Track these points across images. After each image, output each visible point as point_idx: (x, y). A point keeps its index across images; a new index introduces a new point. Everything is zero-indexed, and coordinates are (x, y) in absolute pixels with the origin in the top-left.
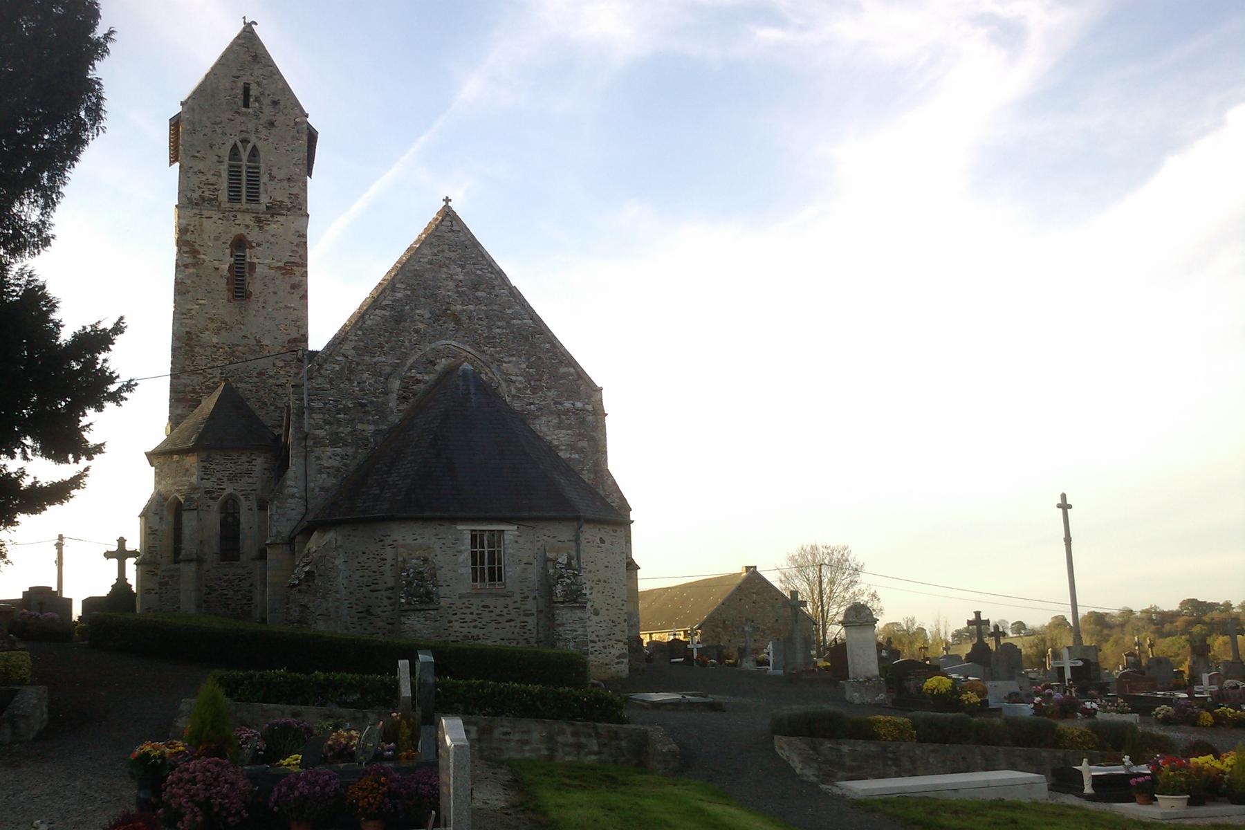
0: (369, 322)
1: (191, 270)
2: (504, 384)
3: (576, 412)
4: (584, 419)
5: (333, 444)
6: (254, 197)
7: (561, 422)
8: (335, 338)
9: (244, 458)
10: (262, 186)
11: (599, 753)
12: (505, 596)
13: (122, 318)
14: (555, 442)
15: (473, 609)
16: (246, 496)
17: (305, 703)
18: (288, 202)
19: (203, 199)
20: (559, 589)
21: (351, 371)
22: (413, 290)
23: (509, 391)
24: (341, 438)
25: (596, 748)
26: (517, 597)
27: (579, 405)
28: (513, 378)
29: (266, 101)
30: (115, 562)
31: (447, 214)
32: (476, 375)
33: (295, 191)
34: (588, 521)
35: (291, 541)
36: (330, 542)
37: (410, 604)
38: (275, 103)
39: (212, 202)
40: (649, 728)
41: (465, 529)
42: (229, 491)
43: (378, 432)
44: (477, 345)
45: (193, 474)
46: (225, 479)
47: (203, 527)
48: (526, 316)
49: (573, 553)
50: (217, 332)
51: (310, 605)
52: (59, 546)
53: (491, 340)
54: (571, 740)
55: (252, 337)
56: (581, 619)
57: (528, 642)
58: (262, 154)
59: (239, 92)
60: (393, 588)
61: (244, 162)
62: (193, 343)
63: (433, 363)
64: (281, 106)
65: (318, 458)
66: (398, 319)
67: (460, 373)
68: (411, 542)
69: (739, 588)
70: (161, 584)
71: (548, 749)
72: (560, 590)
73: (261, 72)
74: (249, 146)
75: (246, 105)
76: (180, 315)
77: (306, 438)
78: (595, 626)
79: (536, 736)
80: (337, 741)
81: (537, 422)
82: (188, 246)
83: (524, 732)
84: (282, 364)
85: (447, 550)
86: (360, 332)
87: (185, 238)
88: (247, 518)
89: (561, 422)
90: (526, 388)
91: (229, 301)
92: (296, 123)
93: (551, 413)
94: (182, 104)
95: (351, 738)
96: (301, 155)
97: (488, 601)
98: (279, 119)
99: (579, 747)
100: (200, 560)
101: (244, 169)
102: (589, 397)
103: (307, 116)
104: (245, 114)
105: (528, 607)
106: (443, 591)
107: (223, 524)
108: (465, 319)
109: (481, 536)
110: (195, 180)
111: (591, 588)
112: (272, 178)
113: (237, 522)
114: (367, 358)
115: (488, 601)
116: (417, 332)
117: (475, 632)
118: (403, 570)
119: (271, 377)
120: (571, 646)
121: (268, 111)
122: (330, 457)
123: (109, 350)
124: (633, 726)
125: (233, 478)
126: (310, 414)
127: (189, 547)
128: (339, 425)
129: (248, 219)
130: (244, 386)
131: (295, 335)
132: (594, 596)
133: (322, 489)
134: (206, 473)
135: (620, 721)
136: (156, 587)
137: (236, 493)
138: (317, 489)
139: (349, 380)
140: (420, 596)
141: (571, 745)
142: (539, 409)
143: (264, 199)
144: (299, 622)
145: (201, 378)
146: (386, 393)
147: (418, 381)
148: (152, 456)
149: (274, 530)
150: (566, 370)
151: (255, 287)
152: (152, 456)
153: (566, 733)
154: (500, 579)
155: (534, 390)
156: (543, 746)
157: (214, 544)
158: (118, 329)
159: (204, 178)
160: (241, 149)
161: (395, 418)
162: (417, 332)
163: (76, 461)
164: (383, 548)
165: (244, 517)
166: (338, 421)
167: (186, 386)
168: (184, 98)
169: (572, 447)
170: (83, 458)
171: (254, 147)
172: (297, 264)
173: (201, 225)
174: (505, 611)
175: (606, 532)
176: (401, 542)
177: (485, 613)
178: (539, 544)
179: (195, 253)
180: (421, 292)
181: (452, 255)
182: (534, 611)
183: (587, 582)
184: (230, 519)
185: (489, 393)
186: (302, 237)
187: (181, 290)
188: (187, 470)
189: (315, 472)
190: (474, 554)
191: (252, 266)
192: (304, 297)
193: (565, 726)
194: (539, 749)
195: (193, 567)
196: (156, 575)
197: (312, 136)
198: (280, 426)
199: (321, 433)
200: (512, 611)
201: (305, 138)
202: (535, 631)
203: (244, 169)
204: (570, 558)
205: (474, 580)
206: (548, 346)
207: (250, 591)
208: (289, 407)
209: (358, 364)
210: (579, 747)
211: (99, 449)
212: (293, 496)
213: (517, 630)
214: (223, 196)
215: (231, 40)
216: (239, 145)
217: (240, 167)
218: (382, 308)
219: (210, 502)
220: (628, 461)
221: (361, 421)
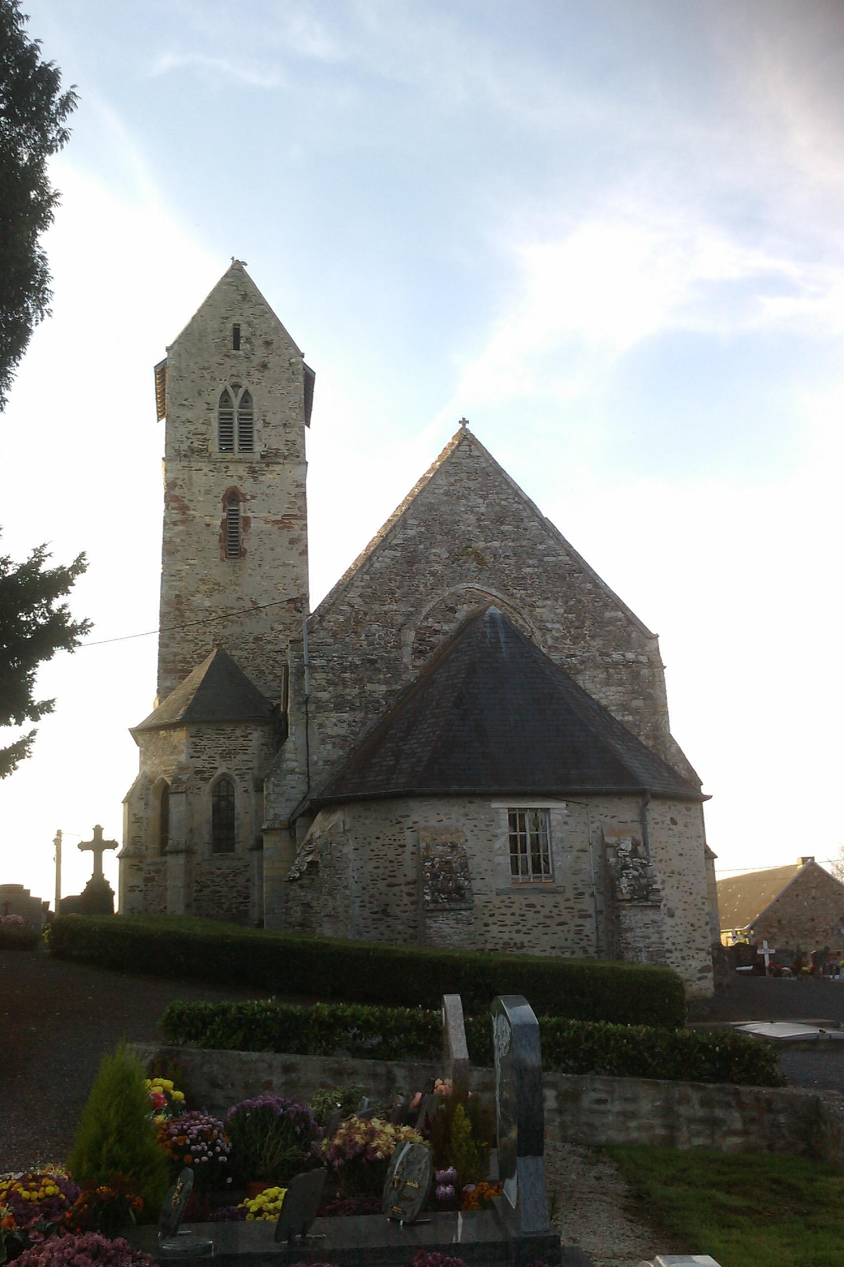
0: (377, 565)
1: (181, 528)
2: (538, 633)
3: (627, 664)
4: (638, 673)
5: (339, 708)
6: (247, 445)
7: (609, 676)
8: (339, 584)
9: (238, 733)
10: (255, 433)
11: (745, 1133)
12: (554, 892)
13: (83, 555)
14: (604, 702)
15: (515, 909)
16: (242, 776)
17: (302, 1050)
18: (284, 450)
19: (192, 450)
20: (624, 883)
21: (358, 622)
22: (428, 527)
23: (545, 642)
24: (348, 701)
25: (739, 1126)
26: (570, 894)
27: (630, 656)
28: (549, 625)
29: (257, 342)
30: (90, 854)
31: (465, 438)
32: (505, 621)
33: (291, 437)
34: (656, 796)
35: (290, 826)
36: (336, 825)
37: (435, 901)
38: (268, 343)
39: (202, 452)
40: (820, 1094)
41: (501, 807)
42: (222, 770)
43: (390, 693)
44: (504, 588)
45: (181, 752)
46: (217, 757)
47: (193, 812)
48: (561, 552)
49: (639, 837)
50: (209, 594)
51: (314, 904)
52: (58, 842)
53: (520, 581)
54: (700, 1112)
55: (247, 598)
56: (653, 922)
57: (586, 952)
58: (255, 399)
59: (229, 333)
60: (414, 882)
61: (236, 409)
62: (183, 607)
63: (453, 610)
64: (274, 346)
65: (321, 726)
66: (411, 561)
67: (486, 618)
68: (433, 822)
69: (796, 882)
70: (147, 880)
71: (667, 1127)
72: (624, 886)
73: (251, 311)
74: (241, 392)
75: (237, 347)
76: (169, 577)
77: (306, 702)
78: (673, 930)
79: (645, 1106)
80: (348, 1139)
81: (580, 677)
82: (177, 501)
83: (626, 1100)
84: (281, 627)
85: (478, 833)
86: (367, 577)
87: (172, 492)
88: (242, 802)
89: (609, 676)
90: (564, 637)
91: (222, 560)
92: (291, 364)
93: (597, 667)
94: (168, 349)
95: (372, 1134)
96: (297, 398)
97: (534, 899)
98: (273, 361)
99: (713, 1123)
100: (189, 851)
101: (236, 416)
102: (643, 646)
103: (303, 356)
104: (236, 357)
105: (584, 907)
106: (477, 885)
107: (216, 809)
108: (489, 558)
109: (522, 817)
110: (183, 430)
111: (663, 882)
112: (266, 424)
113: (231, 806)
114: (376, 607)
115: (534, 899)
116: (433, 574)
117: (518, 938)
118: (426, 858)
119: (269, 642)
120: (643, 957)
121: (260, 353)
122: (335, 724)
123: (68, 592)
124: (802, 1091)
125: (227, 755)
126: (311, 674)
127: (177, 836)
128: (345, 686)
129: (242, 470)
130: (239, 653)
131: (294, 595)
132: (670, 894)
133: (326, 762)
134: (196, 750)
135: (772, 1081)
136: (141, 883)
137: (233, 774)
138: (321, 763)
139: (356, 633)
140: (450, 893)
141: (702, 1121)
142: (582, 662)
143: (258, 448)
144: (302, 925)
145: (192, 646)
146: (399, 646)
147: (436, 632)
148: (138, 733)
149: (272, 812)
150: (613, 614)
151: (249, 543)
152: (138, 733)
153: (692, 1101)
154: (547, 872)
155: (575, 640)
156: (656, 1122)
157: (205, 833)
158: (79, 567)
159: (192, 428)
160: (232, 394)
161: (410, 676)
162: (433, 574)
163: (19, 722)
164: (401, 832)
165: (239, 801)
166: (344, 681)
167: (175, 654)
168: (169, 343)
169: (624, 707)
170: (28, 719)
171: (247, 392)
172: (295, 517)
173: (190, 479)
174: (555, 911)
175: (677, 810)
176: (422, 824)
177: (530, 915)
178: (595, 826)
179: (183, 509)
180: (437, 529)
181: (471, 484)
182: (591, 911)
183: (658, 873)
184: (223, 804)
185: (520, 641)
186: (301, 486)
187: (170, 549)
188: (175, 747)
189: (318, 742)
190: (513, 839)
191: (247, 520)
192: (304, 552)
193: (690, 1091)
194: (652, 1127)
195: (181, 859)
196: (141, 869)
197: (309, 378)
198: (280, 698)
199: (324, 696)
200: (564, 912)
201: (301, 379)
202: (593, 937)
203: (236, 416)
204: (635, 844)
205: (515, 871)
206: (589, 586)
207: (247, 888)
208: (286, 667)
209: (365, 614)
210: (713, 1123)
211: (47, 706)
212: (292, 771)
213: (571, 936)
214: (214, 446)
215: (219, 279)
216: (230, 390)
217: (231, 414)
218: (393, 548)
219: (201, 784)
220: (696, 723)
221: (371, 681)
